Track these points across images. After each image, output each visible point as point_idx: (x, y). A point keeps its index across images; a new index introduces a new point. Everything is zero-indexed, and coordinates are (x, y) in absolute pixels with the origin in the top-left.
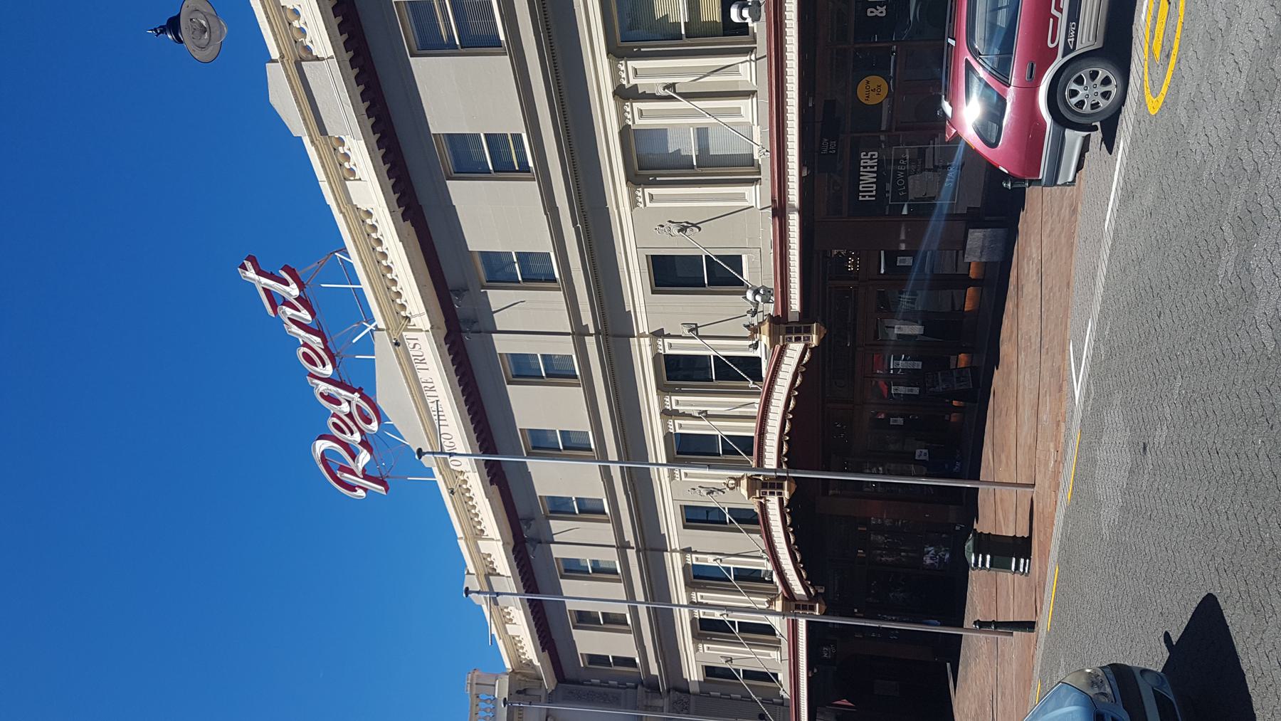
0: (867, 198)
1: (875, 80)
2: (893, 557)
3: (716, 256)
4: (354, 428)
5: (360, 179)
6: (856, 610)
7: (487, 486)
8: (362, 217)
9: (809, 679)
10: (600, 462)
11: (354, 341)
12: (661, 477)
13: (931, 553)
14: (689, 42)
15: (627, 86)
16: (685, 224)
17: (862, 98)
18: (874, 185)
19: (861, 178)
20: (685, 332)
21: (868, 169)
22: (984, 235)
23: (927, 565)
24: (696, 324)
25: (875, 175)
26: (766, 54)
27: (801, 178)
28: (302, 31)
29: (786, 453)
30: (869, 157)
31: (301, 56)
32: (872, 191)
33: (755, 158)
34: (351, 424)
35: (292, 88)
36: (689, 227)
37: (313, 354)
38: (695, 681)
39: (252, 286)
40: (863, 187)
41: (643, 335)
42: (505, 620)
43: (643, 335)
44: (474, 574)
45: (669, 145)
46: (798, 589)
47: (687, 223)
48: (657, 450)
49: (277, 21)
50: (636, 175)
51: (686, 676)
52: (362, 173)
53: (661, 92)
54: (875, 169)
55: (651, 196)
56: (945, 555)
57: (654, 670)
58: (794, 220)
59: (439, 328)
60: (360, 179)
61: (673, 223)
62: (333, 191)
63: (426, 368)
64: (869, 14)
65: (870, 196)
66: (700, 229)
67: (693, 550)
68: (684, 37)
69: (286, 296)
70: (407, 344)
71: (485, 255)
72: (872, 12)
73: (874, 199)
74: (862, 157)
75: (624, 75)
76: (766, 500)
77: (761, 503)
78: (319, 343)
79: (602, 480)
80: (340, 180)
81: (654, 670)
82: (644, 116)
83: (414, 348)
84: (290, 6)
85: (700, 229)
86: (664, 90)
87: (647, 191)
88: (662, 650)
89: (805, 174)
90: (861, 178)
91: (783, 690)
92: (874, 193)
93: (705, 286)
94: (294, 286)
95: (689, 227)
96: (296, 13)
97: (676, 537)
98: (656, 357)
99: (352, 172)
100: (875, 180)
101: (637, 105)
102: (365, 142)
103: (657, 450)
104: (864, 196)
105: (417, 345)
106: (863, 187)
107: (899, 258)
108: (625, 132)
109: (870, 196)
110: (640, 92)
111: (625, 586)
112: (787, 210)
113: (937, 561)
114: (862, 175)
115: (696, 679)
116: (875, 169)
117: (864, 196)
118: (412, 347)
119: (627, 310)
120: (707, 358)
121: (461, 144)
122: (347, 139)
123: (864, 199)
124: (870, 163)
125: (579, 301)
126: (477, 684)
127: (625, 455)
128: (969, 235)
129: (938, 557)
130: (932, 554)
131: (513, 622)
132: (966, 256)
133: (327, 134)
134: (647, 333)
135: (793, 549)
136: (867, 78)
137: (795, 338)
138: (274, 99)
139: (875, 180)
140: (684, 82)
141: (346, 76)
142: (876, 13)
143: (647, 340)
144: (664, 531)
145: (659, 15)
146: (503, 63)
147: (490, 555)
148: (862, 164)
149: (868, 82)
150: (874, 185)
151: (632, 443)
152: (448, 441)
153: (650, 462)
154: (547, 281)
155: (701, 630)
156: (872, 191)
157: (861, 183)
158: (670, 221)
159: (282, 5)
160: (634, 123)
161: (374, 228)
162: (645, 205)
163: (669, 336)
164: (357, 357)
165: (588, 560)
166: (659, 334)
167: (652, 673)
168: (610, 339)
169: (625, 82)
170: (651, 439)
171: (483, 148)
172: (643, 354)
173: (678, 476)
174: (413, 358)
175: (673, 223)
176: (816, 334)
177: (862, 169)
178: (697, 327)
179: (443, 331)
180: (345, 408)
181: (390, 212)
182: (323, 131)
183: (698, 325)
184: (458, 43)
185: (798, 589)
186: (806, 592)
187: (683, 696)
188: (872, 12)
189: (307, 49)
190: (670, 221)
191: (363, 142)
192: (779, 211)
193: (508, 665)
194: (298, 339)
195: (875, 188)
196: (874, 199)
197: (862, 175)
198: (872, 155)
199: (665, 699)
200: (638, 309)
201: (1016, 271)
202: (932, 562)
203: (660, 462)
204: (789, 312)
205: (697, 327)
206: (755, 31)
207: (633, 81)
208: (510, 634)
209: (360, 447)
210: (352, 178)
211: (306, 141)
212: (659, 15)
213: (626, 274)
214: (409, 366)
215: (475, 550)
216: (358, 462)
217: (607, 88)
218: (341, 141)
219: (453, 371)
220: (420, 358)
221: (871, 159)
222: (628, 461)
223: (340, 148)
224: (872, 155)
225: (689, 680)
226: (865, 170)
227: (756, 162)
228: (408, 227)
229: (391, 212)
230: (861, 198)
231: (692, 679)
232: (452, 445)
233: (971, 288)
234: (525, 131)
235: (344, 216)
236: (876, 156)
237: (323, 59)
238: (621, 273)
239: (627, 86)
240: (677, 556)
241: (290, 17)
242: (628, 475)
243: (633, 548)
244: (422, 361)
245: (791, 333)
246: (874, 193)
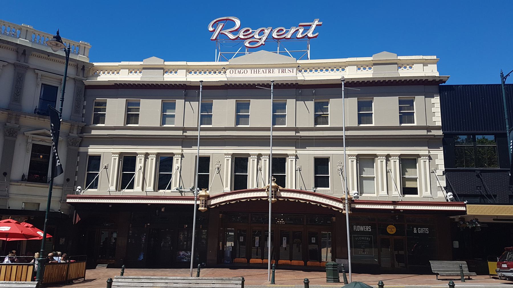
0: (354, 228)
1: (394, 230)
2: (183, 239)
3: (98, 175)
4: (246, 37)
5: (129, 74)
6: (149, 224)
7: (244, 82)
8: (342, 67)
9: (147, 204)
10: (272, 128)
11: (216, 50)
12: (154, 150)
13: (187, 254)
14: (121, 174)
15: (148, 156)
16: (219, 169)
17: (389, 226)
18: (359, 230)
19: (362, 226)
20: (298, 167)
21: (365, 228)
22: (346, 264)
23: (179, 253)
24: (108, 168)
25: (363, 230)
26: (186, 196)
27: (147, 204)
28: (405, 68)
29: (251, 200)
30: (369, 229)
31: (400, 65)
32: (357, 229)
33: (363, 194)
34: (249, 36)
35: (391, 60)
36: (218, 170)
37: (283, 33)
38: (88, 150)
39: (313, 21)
40: (358, 227)
41: (182, 151)
42: (360, 66)
43: (182, 151)
44: (296, 62)
45: (366, 168)
46: (213, 202)
47: (220, 170)
48: (205, 151)
49: (410, 62)
50: (159, 155)
51: (91, 146)
52: (130, 75)
53: (259, 167)
54: (365, 231)
55: (178, 159)
56: (186, 259)
57: (94, 132)
58: (391, 207)
59: (190, 83)
60: (129, 74)
61: (220, 165)
62: (351, 61)
63: (267, 73)
64: (414, 228)
65: (355, 229)
66: (218, 173)
67: (182, 158)
68: (402, 176)
69: (308, 31)
70: (291, 69)
71: (285, 104)
72: (415, 229)
73: (354, 230)
74: (369, 227)
75: (253, 157)
76: (267, 192)
77: (265, 190)
78: (287, 37)
79: (225, 127)
80: (129, 68)
81: (94, 132)
82: (379, 163)
83: (289, 70)
84: (413, 66)
85: (218, 173)
86: (218, 167)
87: (118, 158)
88: (114, 138)
89: (401, 211)
90: (362, 226)
91: (84, 192)
92: (356, 230)
93: (87, 171)
94: (301, 36)
95: (218, 170)
96: (411, 67)
97: (190, 152)
98: (173, 154)
99: (131, 72)
100: (361, 230)
101: (143, 158)
102: (372, 78)
103: (205, 151)
104: (355, 227)
105: (290, 72)
106: (358, 227)
107: (286, 238)
108: (376, 156)
109: (355, 229)
110: (259, 161)
111: (137, 127)
112: (395, 206)
113: (182, 257)
114: (363, 227)
115: (89, 151)
116: (365, 231)
117: (355, 227)
118: (289, 70)
119: (193, 147)
120: (171, 171)
121: (368, 105)
122: (141, 75)
123: (354, 227)
124: (367, 229)
125: (324, 131)
126: (85, 47)
127: (275, 138)
128: (346, 260)
129: (184, 257)
130: (186, 255)
131: (129, 73)
132: (338, 259)
133: (374, 65)
134: (183, 152)
135: (237, 200)
136: (388, 227)
137: (203, 203)
138: (154, 58)
139: (361, 230)
140: (392, 174)
141: (398, 78)
142: (415, 230)
143: (181, 152)
144: (307, 148)
145: (408, 170)
146: (233, 125)
147: (118, 73)
148: (367, 227)
149: (394, 228)
150: (359, 230)
151: (207, 141)
152: (243, 71)
153: (200, 147)
154: (127, 122)
155: (124, 156)
156: (357, 229)
157: (360, 226)
158: (221, 165)
159: (414, 65)
160: (138, 157)
161: (113, 73)
162: (113, 156)
163: (181, 159)
164: (216, 50)
165: (175, 113)
166: (182, 156)
167: (92, 131)
168: (182, 140)
169: (150, 156)
170: (309, 149)
171: (411, 112)
172: (176, 150)
173: (265, 157)
174: (284, 69)
175: (220, 165)
176: (204, 209)
177: (365, 226)
178: (106, 169)
179: (188, 84)
180: (257, 36)
181: (352, 78)
182: (144, 69)
183: (107, 169)
184: (360, 112)
185: (213, 202)
186: (212, 205)
187: (78, 143)
188: (415, 229)
189: (401, 67)
190: (221, 165)
191: (140, 80)
192: (394, 203)
193: (95, 64)
194: (256, 30)
195: (358, 230)
196: (354, 230)
197: (363, 227)
198: (370, 229)
199: (77, 135)
200: (192, 150)
201: (258, 273)
202: (181, 254)
203: (272, 151)
204: (355, 204)
205: (106, 169)
206: (159, 192)
207: (150, 158)
208: (121, 70)
209: (236, 36)
210: (357, 68)
211: (141, 63)
212: (408, 170)
213: (322, 149)
214: (283, 67)
215: (180, 67)
216: (228, 33)
217: (149, 151)
218: (140, 72)
219: (172, 84)
220: (284, 71)
221: (368, 229)
222: (200, 139)
223: (174, 72)
224: (370, 229)
225: (89, 147)
226: (423, 230)
227: (362, 194)
228: (431, 79)
229: (352, 79)
230: (354, 226)
231: (89, 149)
232: (241, 73)
233: (304, 262)
234: (175, 126)
235: (344, 62)
236: (369, 231)
237: (163, 76)
238: (322, 147)
239: (148, 156)
240: (180, 151)
241: (104, 71)
242: (195, 138)
243: (183, 134)
244: (269, 72)
245: (205, 202)
246: (356, 230)
